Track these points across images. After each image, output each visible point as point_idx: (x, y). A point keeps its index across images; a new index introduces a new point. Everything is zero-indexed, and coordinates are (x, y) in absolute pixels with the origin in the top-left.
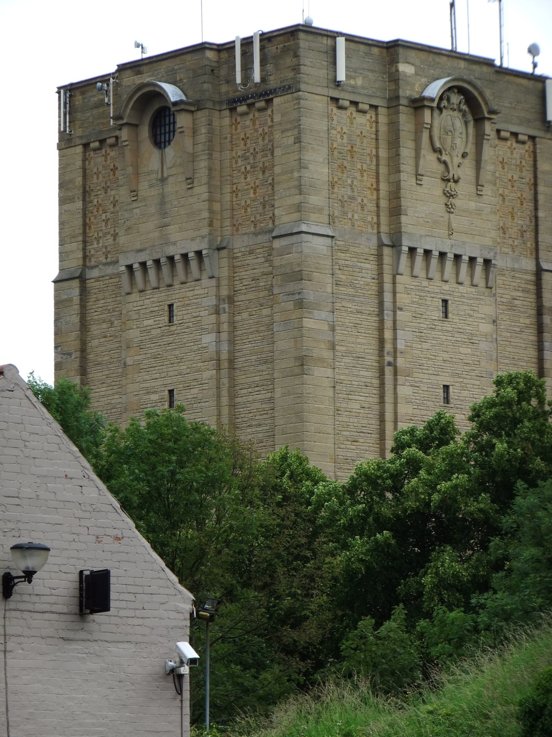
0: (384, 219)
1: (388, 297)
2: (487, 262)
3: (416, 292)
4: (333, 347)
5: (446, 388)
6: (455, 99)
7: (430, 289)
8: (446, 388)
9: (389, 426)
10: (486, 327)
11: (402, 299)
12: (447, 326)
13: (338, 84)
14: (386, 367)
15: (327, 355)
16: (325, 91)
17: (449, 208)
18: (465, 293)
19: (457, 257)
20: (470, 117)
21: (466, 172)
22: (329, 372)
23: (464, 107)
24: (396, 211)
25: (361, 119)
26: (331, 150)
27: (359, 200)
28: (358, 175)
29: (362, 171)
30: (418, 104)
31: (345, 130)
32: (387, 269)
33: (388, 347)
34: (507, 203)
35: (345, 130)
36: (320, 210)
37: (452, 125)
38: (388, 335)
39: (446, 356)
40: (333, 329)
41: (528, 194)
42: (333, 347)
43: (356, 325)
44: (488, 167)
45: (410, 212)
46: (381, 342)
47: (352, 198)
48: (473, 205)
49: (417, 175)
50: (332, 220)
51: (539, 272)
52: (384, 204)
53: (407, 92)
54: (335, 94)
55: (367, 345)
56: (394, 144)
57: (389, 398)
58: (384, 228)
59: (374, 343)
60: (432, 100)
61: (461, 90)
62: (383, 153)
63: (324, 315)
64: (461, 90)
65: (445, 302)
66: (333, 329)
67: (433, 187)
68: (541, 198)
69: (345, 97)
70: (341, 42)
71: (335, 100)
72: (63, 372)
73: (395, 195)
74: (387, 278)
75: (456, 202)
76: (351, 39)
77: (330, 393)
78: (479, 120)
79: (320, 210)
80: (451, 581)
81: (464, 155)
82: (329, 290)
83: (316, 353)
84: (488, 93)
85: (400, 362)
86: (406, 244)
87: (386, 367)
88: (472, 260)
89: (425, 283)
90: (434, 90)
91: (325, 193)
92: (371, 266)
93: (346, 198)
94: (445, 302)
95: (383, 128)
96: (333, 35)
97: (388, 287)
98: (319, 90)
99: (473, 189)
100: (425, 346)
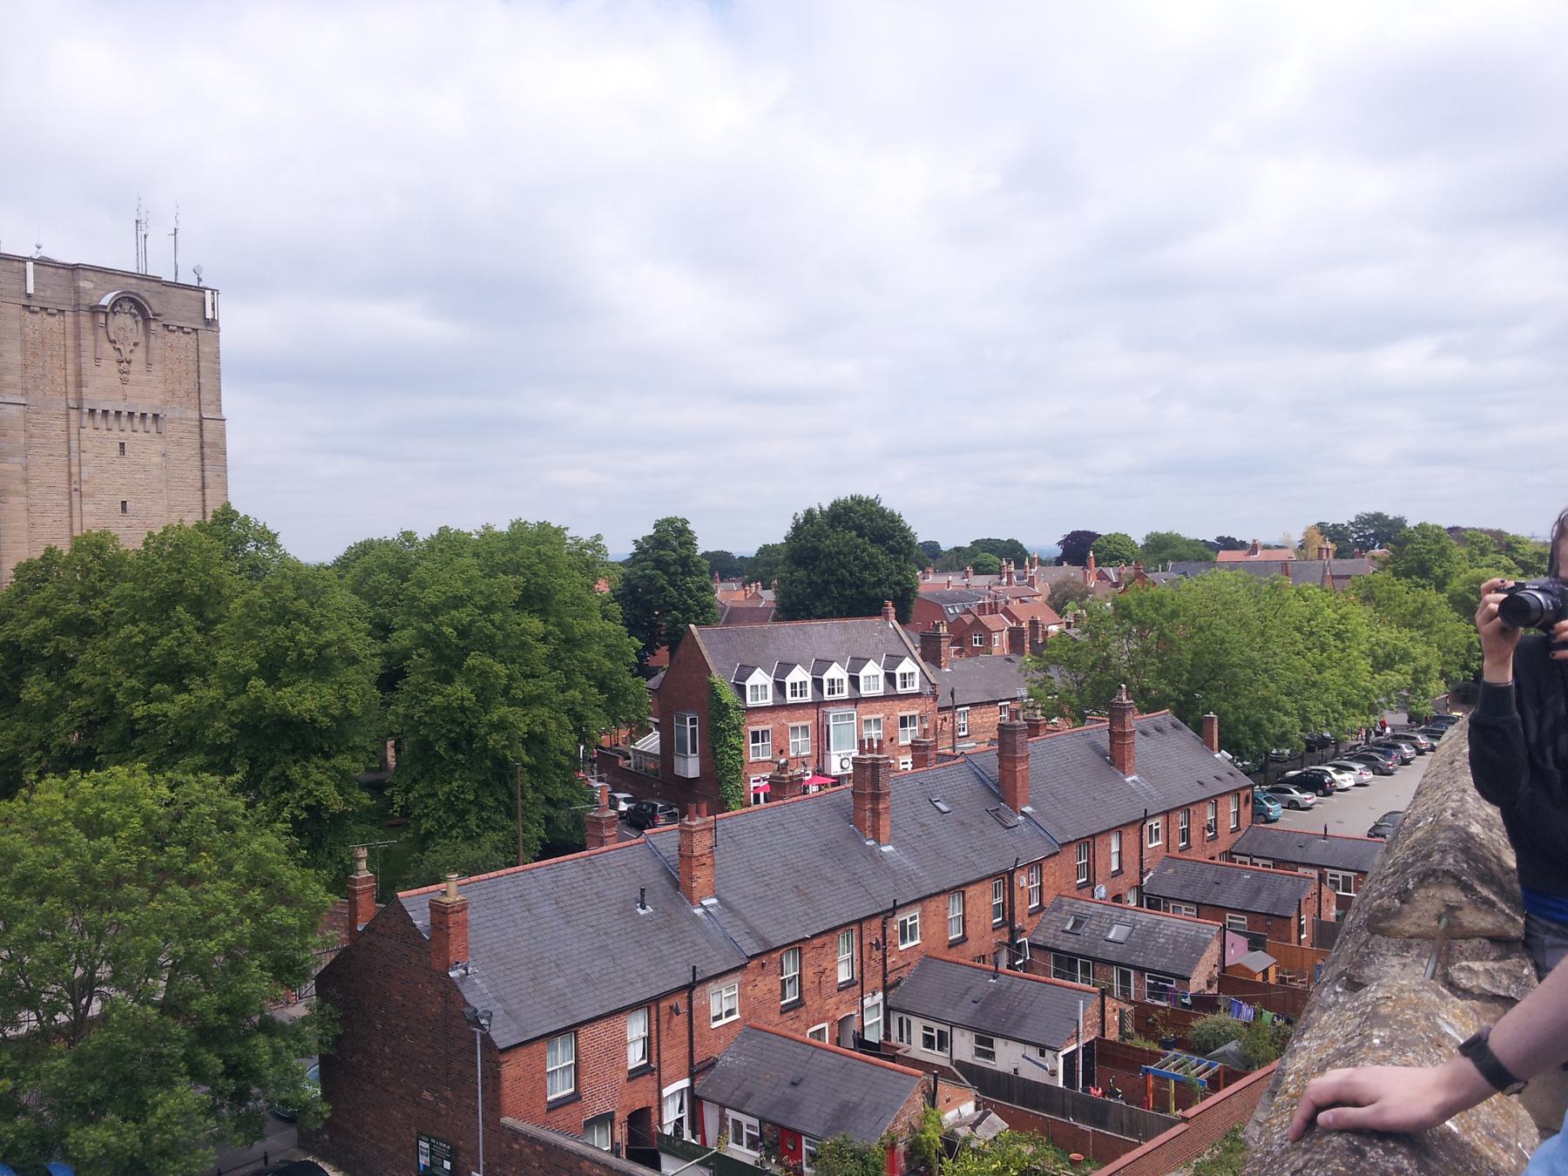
0: (71, 389)
1: (74, 444)
2: (156, 416)
3: (97, 441)
4: (26, 481)
5: (124, 503)
6: (127, 306)
8: (124, 503)
9: (76, 521)
10: (157, 460)
11: (86, 445)
13: (29, 296)
14: (75, 491)
15: (21, 487)
17: (124, 382)
18: (141, 440)
19: (131, 414)
21: (139, 356)
22: (24, 500)
24: (79, 385)
25: (50, 319)
26: (24, 342)
29: (52, 356)
30: (95, 310)
32: (73, 424)
33: (75, 478)
36: (15, 386)
37: (125, 322)
38: (74, 470)
40: (26, 469)
41: (193, 367)
42: (26, 481)
44: (157, 353)
46: (70, 474)
48: (144, 378)
49: (97, 359)
51: (201, 419)
52: (71, 379)
53: (86, 301)
55: (60, 479)
56: (77, 337)
57: (76, 513)
58: (71, 396)
59: (65, 476)
61: (131, 300)
62: (70, 343)
63: (17, 460)
64: (131, 300)
65: (122, 445)
66: (26, 469)
67: (110, 368)
68: (202, 370)
69: (35, 305)
70: (30, 265)
71: (26, 307)
73: (79, 373)
74: (74, 431)
75: (130, 377)
76: (41, 262)
77: (25, 514)
78: (147, 320)
79: (15, 386)
80: (392, 560)
81: (135, 344)
82: (22, 441)
83: (11, 487)
84: (153, 302)
85: (84, 488)
86: (86, 407)
87: (75, 491)
88: (143, 415)
90: (106, 300)
92: (62, 423)
94: (122, 445)
95: (70, 326)
96: (24, 260)
97: (74, 436)
99: (143, 367)
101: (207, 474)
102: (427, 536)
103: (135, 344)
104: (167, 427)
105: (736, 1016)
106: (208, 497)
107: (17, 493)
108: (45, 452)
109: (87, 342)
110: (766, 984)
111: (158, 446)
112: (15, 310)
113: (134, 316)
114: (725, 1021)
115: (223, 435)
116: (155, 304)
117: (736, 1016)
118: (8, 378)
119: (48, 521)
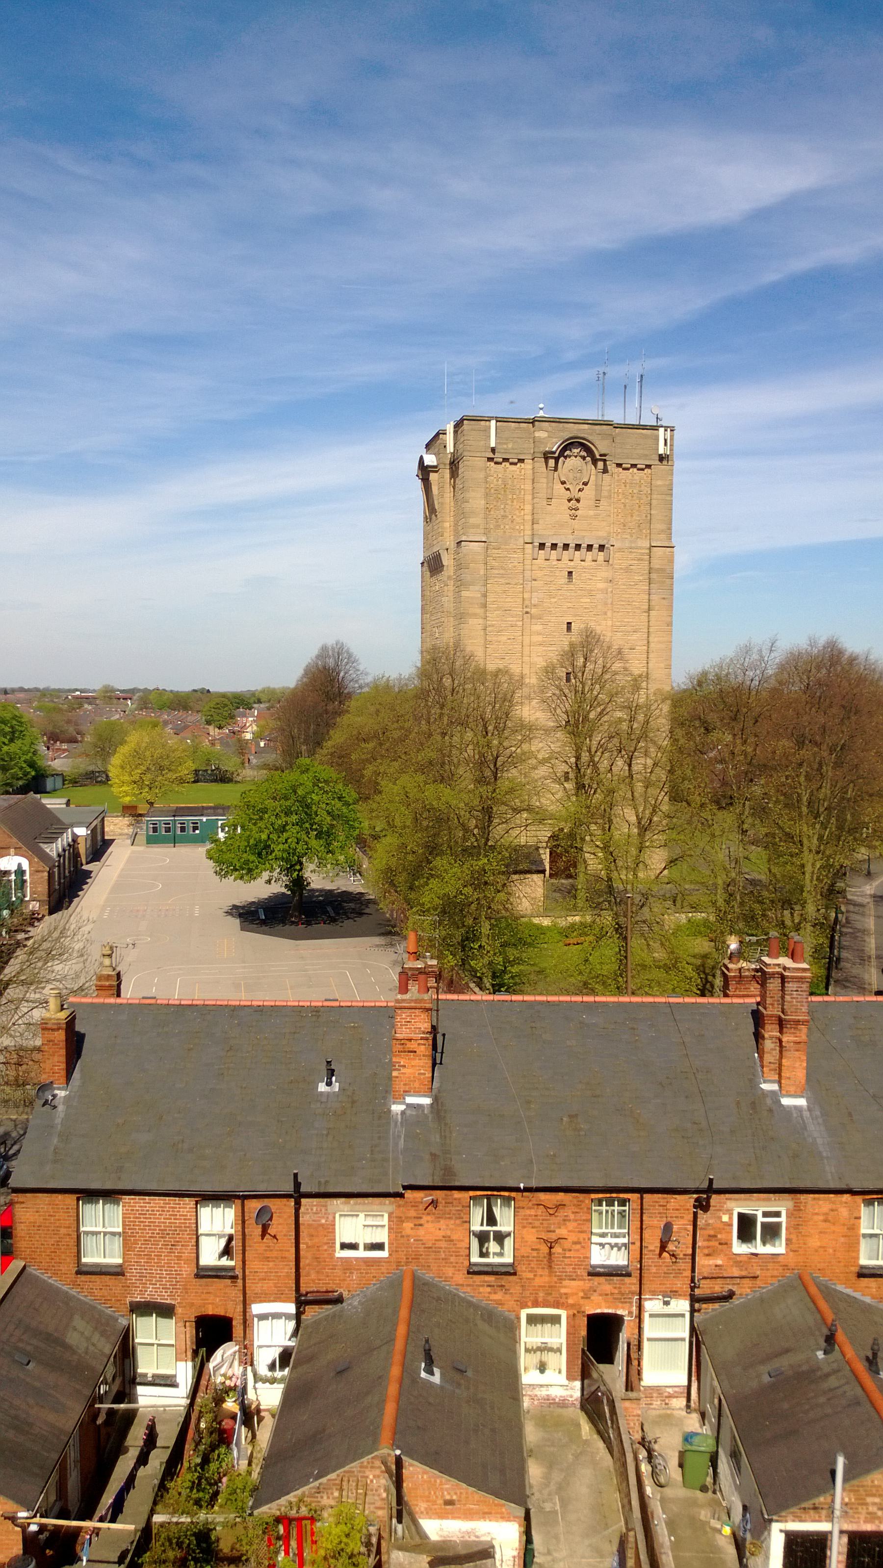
4: (485, 606)
7: (559, 566)
8: (569, 624)
12: (571, 587)
15: (480, 611)
16: (484, 454)
20: (588, 459)
22: (481, 621)
23: (584, 453)
27: (510, 517)
28: (509, 502)
31: (500, 476)
34: (627, 507)
35: (500, 476)
36: (478, 526)
39: (570, 605)
40: (485, 596)
43: (505, 591)
45: (540, 522)
47: (504, 517)
48: (591, 513)
50: (487, 531)
54: (491, 456)
60: (554, 453)
61: (582, 445)
63: (477, 588)
65: (570, 573)
72: (667, 483)
77: (482, 633)
82: (482, 572)
83: (471, 611)
89: (555, 563)
91: (482, 516)
93: (500, 517)
94: (570, 573)
98: (478, 454)
100: (553, 600)
101: (653, 597)
102: (413, 670)
103: (585, 484)
104: (616, 557)
105: (384, 1254)
106: (652, 619)
107: (475, 615)
108: (503, 581)
109: (542, 483)
110: (433, 1229)
111: (605, 573)
112: (481, 462)
113: (584, 458)
114: (361, 1253)
115: (671, 561)
116: (600, 446)
117: (384, 1254)
118: (472, 521)
119: (504, 639)
